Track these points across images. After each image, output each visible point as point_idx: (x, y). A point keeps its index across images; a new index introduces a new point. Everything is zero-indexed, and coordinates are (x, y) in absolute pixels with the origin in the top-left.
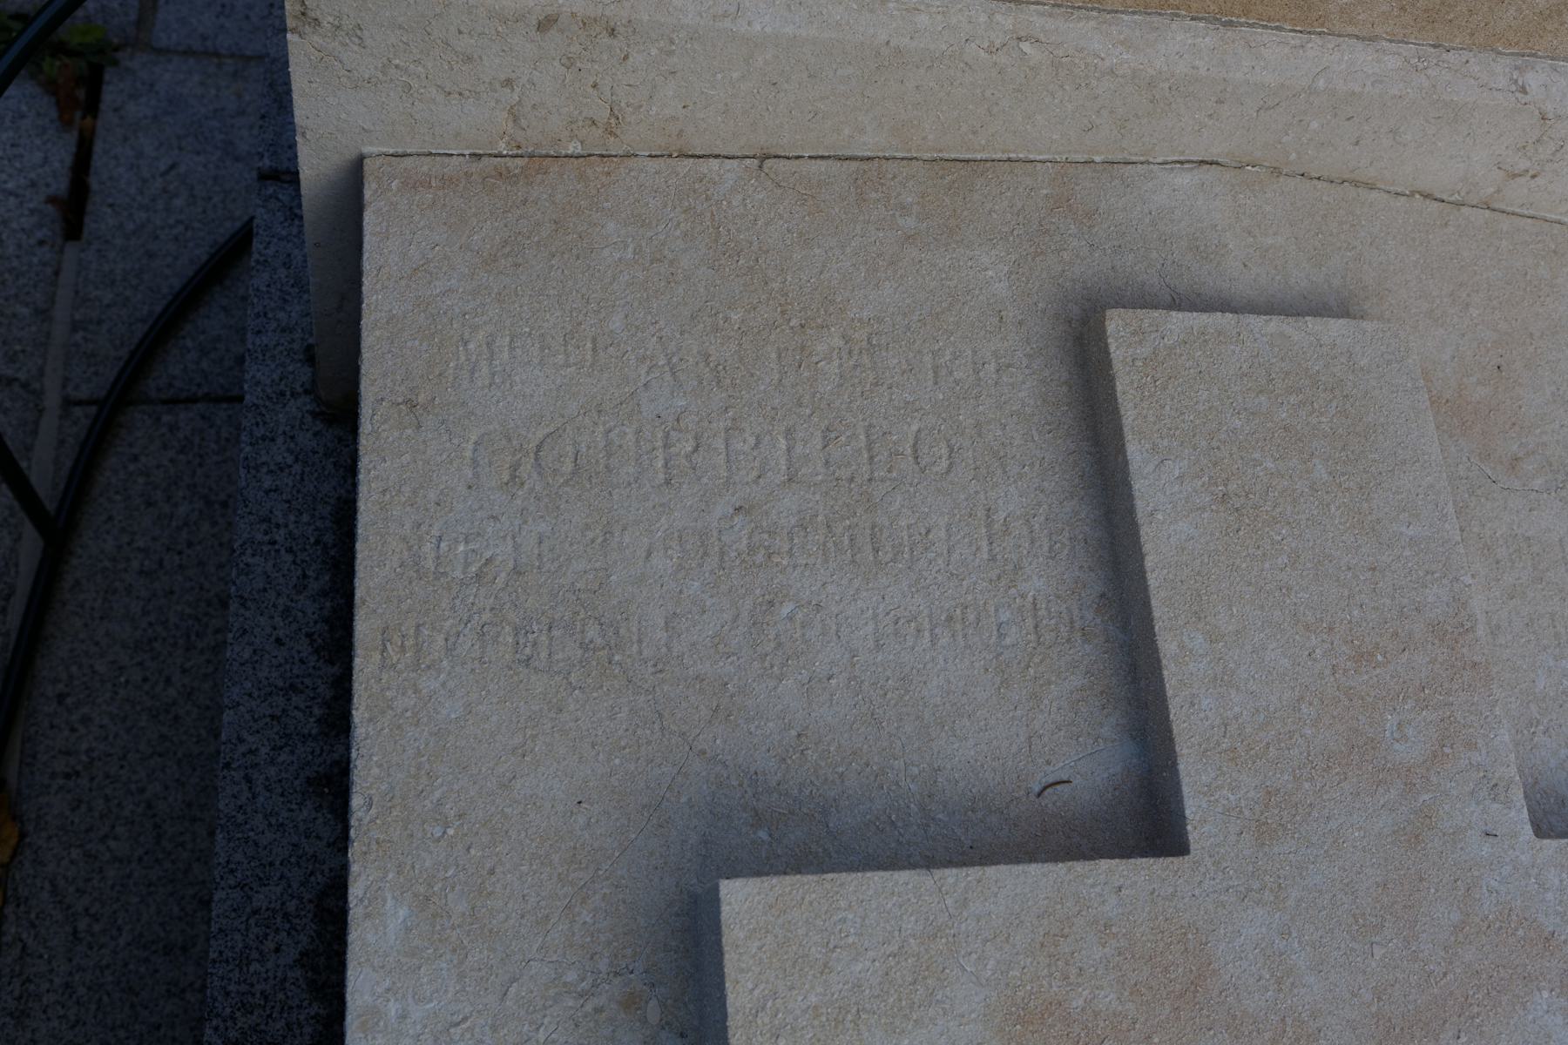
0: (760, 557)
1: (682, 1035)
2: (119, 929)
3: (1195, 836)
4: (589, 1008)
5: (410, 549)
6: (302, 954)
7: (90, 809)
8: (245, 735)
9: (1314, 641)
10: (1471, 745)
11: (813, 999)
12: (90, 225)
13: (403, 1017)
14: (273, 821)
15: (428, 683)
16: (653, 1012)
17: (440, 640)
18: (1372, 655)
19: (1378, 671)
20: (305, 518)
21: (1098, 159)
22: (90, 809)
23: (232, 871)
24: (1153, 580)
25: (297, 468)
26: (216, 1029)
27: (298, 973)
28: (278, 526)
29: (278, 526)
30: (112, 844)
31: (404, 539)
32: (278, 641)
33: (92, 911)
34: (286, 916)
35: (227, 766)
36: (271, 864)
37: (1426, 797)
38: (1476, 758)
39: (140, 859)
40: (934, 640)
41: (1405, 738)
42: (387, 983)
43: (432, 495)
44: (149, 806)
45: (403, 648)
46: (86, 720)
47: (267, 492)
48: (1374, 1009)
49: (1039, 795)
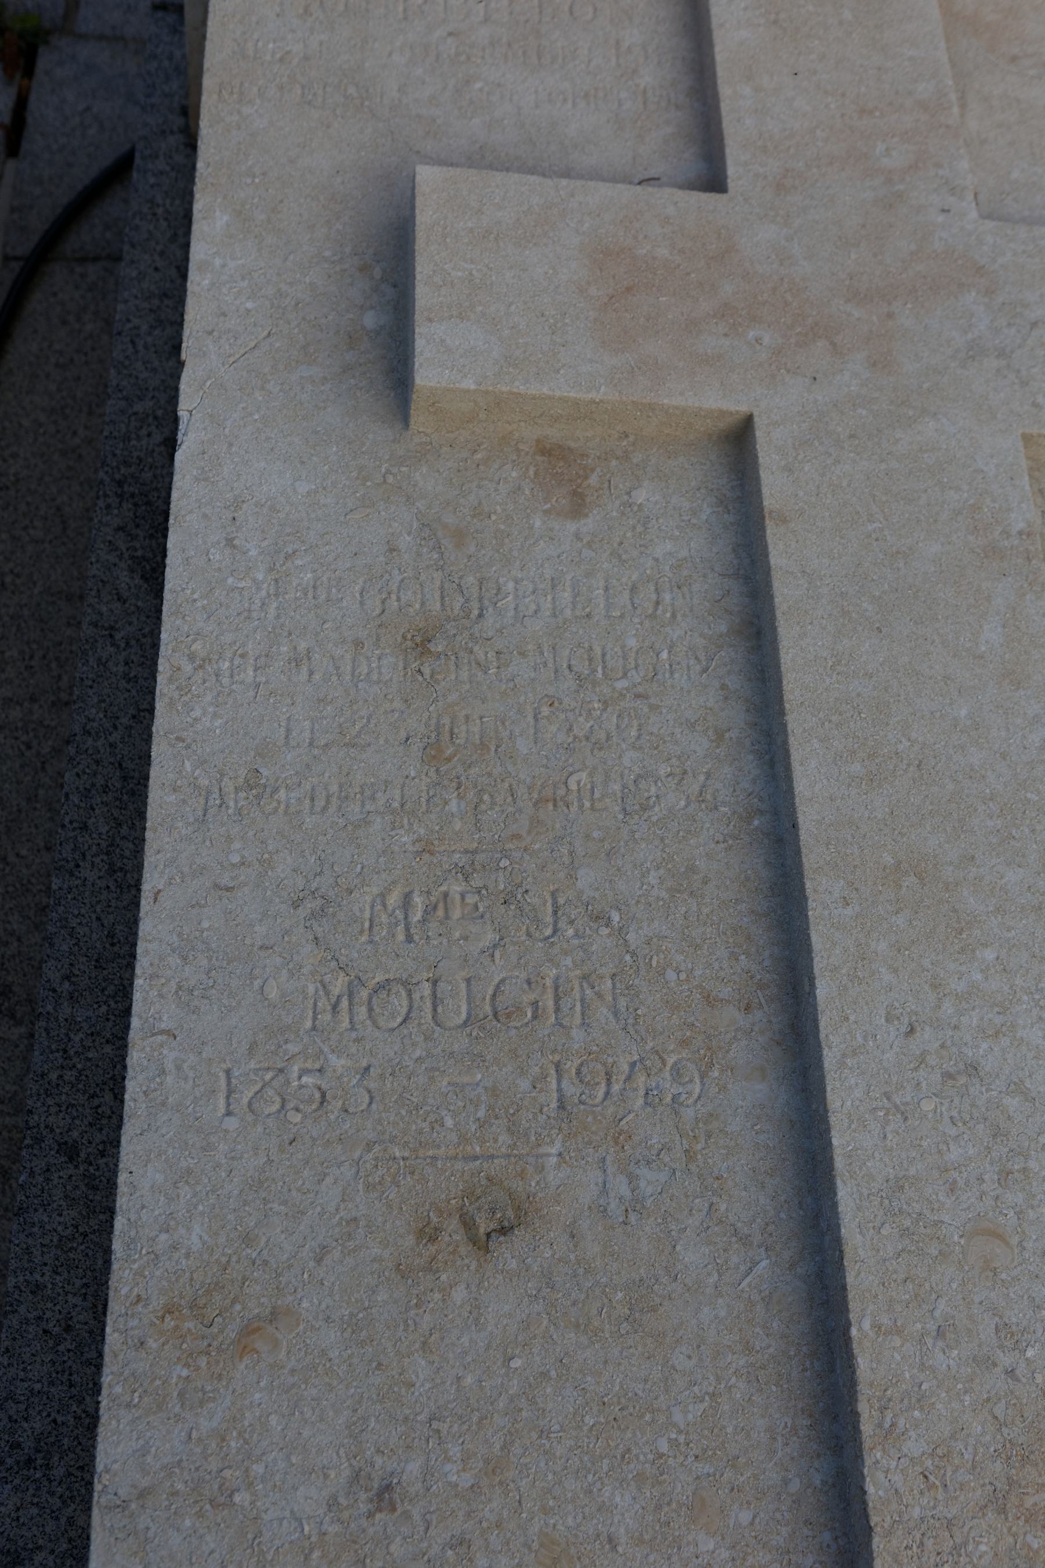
0: (463, 58)
1: (395, 286)
2: (35, 583)
3: (731, 184)
4: (338, 269)
5: (239, 45)
6: (165, 440)
7: (16, 509)
8: (131, 318)
11: (470, 224)
12: (25, 146)
13: (224, 266)
14: (149, 366)
15: (247, 110)
16: (377, 272)
17: (255, 89)
20: (177, 202)
22: (16, 509)
23: (120, 391)
24: (719, 58)
25: (173, 174)
26: (107, 472)
27: (162, 448)
28: (158, 205)
29: (158, 205)
30: (31, 532)
31: (235, 40)
32: (156, 269)
33: (16, 571)
34: (156, 418)
35: (119, 334)
36: (147, 389)
39: (51, 542)
40: (574, 105)
42: (215, 250)
43: (254, 19)
44: (59, 509)
45: (232, 93)
46: (15, 456)
47: (152, 186)
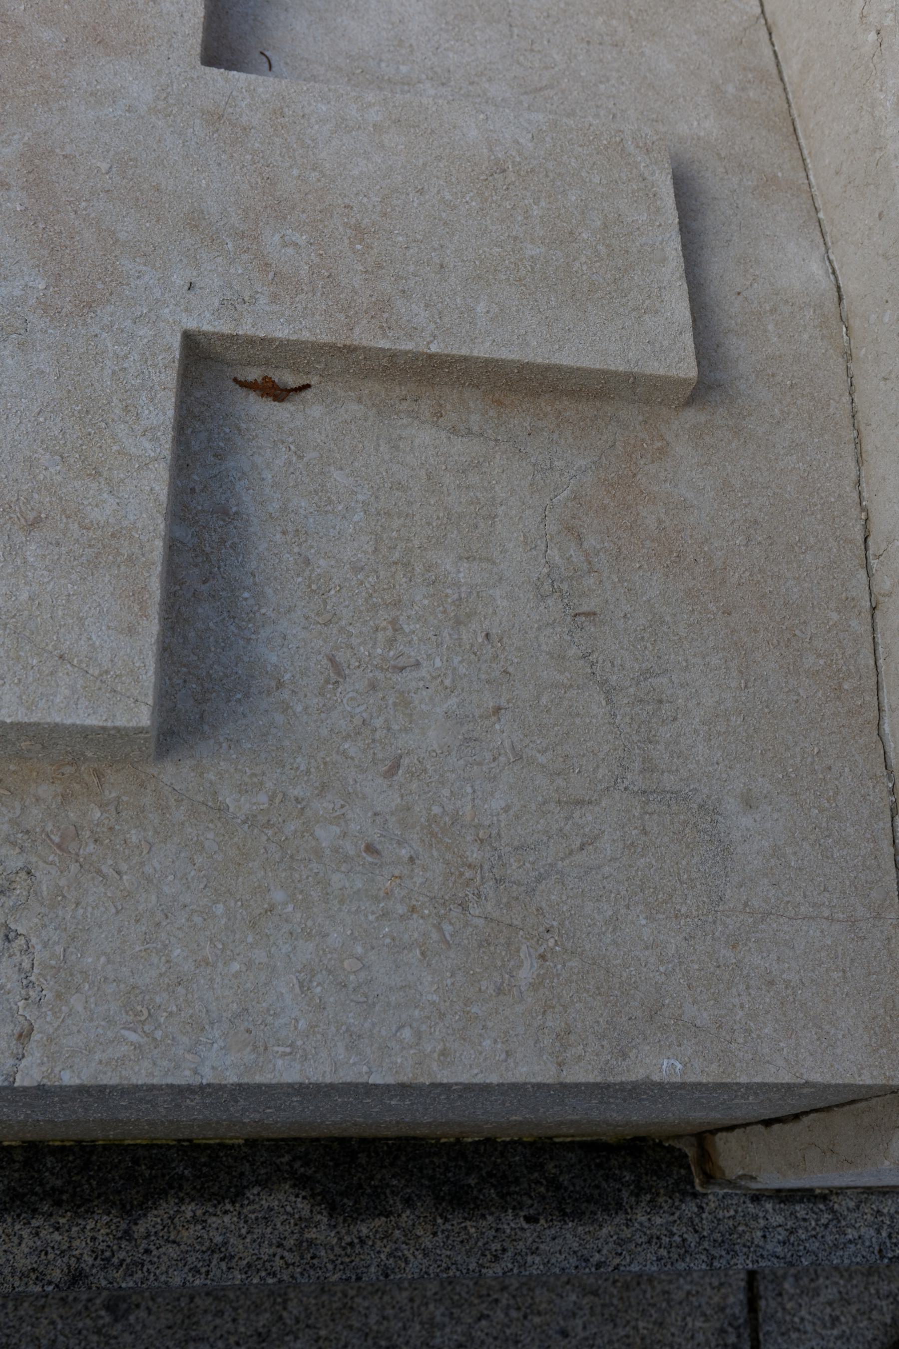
9: (374, 199)
10: (274, 298)
18: (362, 240)
19: (347, 241)
21: (821, 215)
37: (230, 245)
38: (263, 300)
41: (285, 245)
48: (58, 150)
49: (262, 53)
